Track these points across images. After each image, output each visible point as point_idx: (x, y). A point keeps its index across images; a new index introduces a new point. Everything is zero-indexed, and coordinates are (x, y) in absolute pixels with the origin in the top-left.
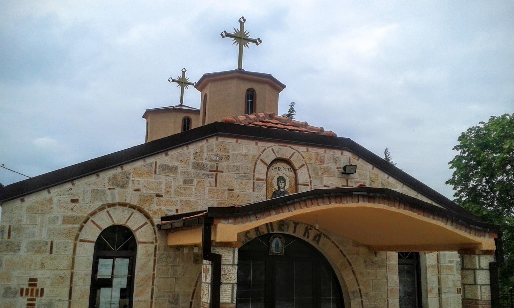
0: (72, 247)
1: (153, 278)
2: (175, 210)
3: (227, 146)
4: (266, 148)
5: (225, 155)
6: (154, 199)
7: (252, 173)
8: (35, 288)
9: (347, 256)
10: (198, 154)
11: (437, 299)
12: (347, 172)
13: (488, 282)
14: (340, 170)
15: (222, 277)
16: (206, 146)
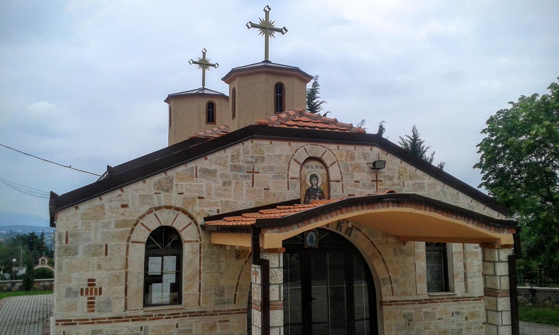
0: (125, 248)
1: (200, 274)
2: (217, 211)
3: (262, 148)
4: (299, 148)
5: (260, 157)
6: (197, 201)
7: (287, 172)
8: (94, 287)
9: (378, 247)
10: (235, 157)
11: (463, 283)
12: (376, 167)
13: (507, 273)
14: (369, 165)
15: (270, 279)
16: (242, 148)
